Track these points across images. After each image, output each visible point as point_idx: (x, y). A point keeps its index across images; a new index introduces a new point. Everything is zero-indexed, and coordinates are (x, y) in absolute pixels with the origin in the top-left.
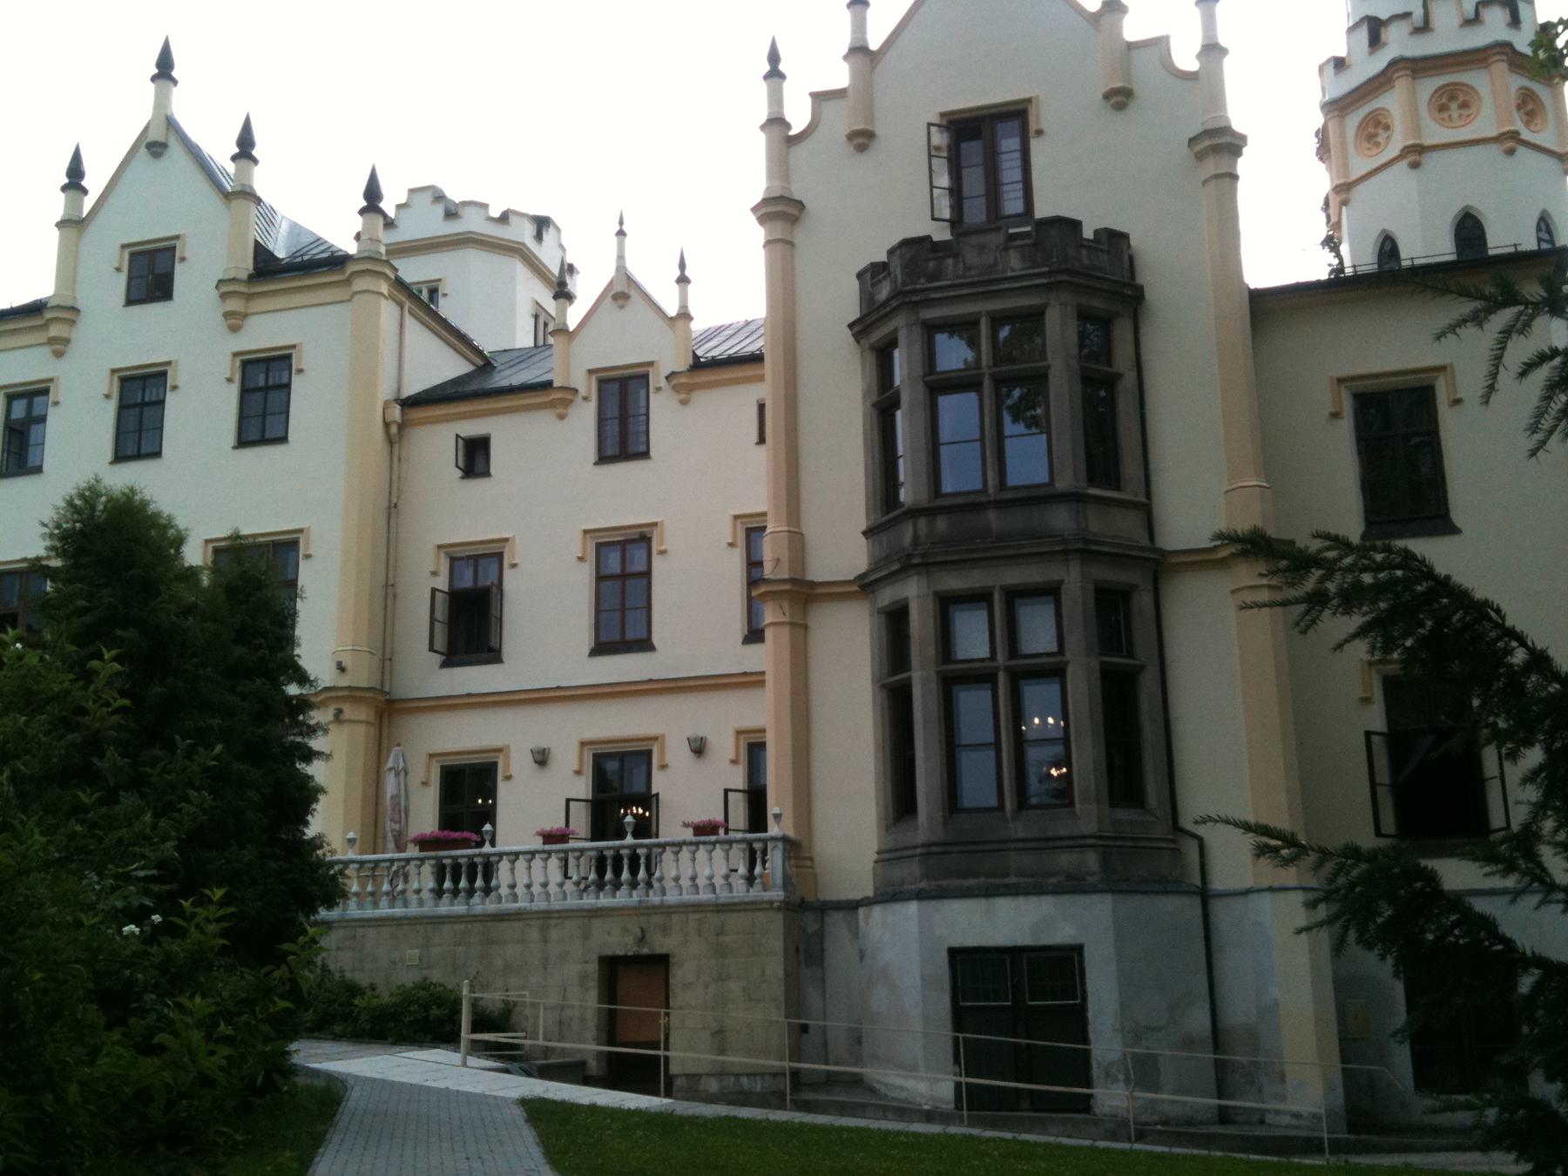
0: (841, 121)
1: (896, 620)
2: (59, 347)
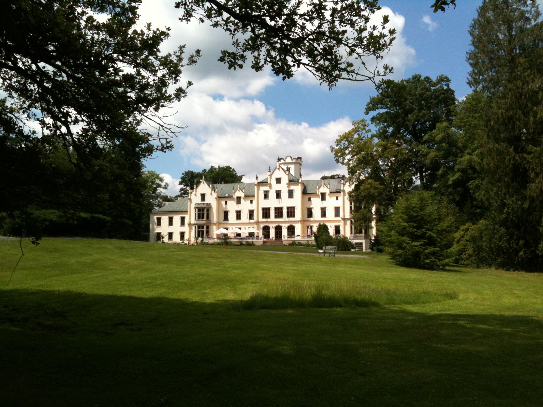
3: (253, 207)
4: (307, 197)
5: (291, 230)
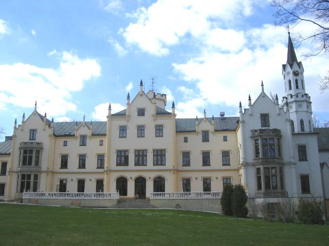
0: (21, 128)
1: (258, 170)
2: (128, 121)
3: (103, 150)
4: (182, 137)
5: (159, 185)
